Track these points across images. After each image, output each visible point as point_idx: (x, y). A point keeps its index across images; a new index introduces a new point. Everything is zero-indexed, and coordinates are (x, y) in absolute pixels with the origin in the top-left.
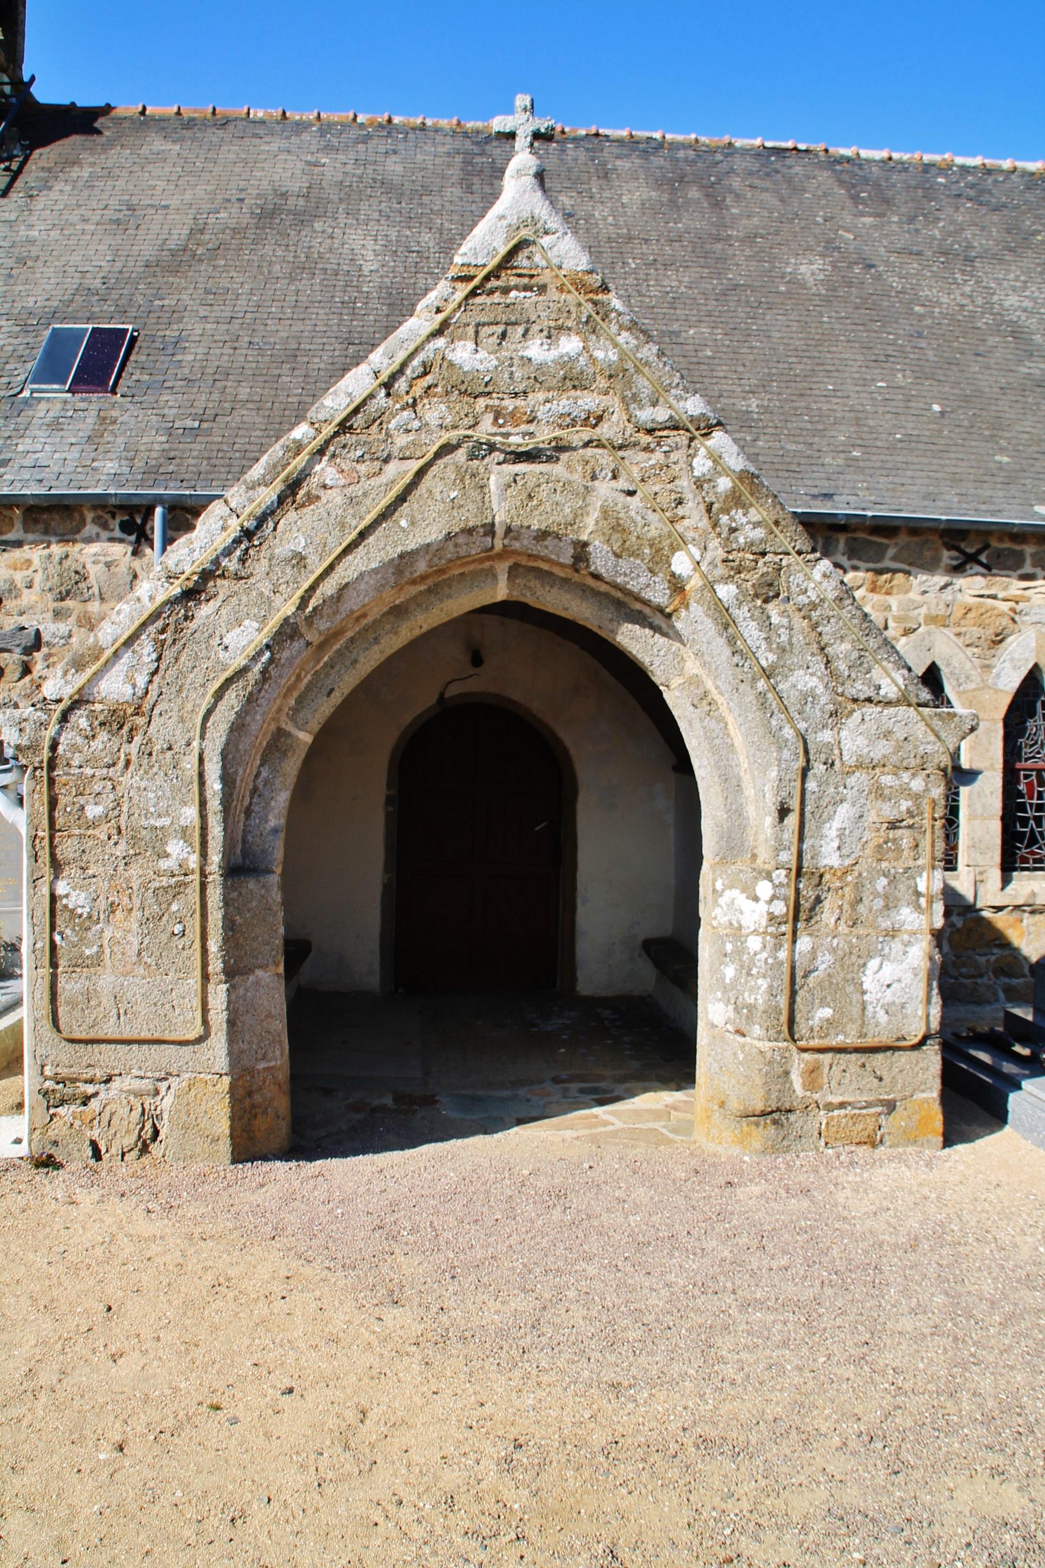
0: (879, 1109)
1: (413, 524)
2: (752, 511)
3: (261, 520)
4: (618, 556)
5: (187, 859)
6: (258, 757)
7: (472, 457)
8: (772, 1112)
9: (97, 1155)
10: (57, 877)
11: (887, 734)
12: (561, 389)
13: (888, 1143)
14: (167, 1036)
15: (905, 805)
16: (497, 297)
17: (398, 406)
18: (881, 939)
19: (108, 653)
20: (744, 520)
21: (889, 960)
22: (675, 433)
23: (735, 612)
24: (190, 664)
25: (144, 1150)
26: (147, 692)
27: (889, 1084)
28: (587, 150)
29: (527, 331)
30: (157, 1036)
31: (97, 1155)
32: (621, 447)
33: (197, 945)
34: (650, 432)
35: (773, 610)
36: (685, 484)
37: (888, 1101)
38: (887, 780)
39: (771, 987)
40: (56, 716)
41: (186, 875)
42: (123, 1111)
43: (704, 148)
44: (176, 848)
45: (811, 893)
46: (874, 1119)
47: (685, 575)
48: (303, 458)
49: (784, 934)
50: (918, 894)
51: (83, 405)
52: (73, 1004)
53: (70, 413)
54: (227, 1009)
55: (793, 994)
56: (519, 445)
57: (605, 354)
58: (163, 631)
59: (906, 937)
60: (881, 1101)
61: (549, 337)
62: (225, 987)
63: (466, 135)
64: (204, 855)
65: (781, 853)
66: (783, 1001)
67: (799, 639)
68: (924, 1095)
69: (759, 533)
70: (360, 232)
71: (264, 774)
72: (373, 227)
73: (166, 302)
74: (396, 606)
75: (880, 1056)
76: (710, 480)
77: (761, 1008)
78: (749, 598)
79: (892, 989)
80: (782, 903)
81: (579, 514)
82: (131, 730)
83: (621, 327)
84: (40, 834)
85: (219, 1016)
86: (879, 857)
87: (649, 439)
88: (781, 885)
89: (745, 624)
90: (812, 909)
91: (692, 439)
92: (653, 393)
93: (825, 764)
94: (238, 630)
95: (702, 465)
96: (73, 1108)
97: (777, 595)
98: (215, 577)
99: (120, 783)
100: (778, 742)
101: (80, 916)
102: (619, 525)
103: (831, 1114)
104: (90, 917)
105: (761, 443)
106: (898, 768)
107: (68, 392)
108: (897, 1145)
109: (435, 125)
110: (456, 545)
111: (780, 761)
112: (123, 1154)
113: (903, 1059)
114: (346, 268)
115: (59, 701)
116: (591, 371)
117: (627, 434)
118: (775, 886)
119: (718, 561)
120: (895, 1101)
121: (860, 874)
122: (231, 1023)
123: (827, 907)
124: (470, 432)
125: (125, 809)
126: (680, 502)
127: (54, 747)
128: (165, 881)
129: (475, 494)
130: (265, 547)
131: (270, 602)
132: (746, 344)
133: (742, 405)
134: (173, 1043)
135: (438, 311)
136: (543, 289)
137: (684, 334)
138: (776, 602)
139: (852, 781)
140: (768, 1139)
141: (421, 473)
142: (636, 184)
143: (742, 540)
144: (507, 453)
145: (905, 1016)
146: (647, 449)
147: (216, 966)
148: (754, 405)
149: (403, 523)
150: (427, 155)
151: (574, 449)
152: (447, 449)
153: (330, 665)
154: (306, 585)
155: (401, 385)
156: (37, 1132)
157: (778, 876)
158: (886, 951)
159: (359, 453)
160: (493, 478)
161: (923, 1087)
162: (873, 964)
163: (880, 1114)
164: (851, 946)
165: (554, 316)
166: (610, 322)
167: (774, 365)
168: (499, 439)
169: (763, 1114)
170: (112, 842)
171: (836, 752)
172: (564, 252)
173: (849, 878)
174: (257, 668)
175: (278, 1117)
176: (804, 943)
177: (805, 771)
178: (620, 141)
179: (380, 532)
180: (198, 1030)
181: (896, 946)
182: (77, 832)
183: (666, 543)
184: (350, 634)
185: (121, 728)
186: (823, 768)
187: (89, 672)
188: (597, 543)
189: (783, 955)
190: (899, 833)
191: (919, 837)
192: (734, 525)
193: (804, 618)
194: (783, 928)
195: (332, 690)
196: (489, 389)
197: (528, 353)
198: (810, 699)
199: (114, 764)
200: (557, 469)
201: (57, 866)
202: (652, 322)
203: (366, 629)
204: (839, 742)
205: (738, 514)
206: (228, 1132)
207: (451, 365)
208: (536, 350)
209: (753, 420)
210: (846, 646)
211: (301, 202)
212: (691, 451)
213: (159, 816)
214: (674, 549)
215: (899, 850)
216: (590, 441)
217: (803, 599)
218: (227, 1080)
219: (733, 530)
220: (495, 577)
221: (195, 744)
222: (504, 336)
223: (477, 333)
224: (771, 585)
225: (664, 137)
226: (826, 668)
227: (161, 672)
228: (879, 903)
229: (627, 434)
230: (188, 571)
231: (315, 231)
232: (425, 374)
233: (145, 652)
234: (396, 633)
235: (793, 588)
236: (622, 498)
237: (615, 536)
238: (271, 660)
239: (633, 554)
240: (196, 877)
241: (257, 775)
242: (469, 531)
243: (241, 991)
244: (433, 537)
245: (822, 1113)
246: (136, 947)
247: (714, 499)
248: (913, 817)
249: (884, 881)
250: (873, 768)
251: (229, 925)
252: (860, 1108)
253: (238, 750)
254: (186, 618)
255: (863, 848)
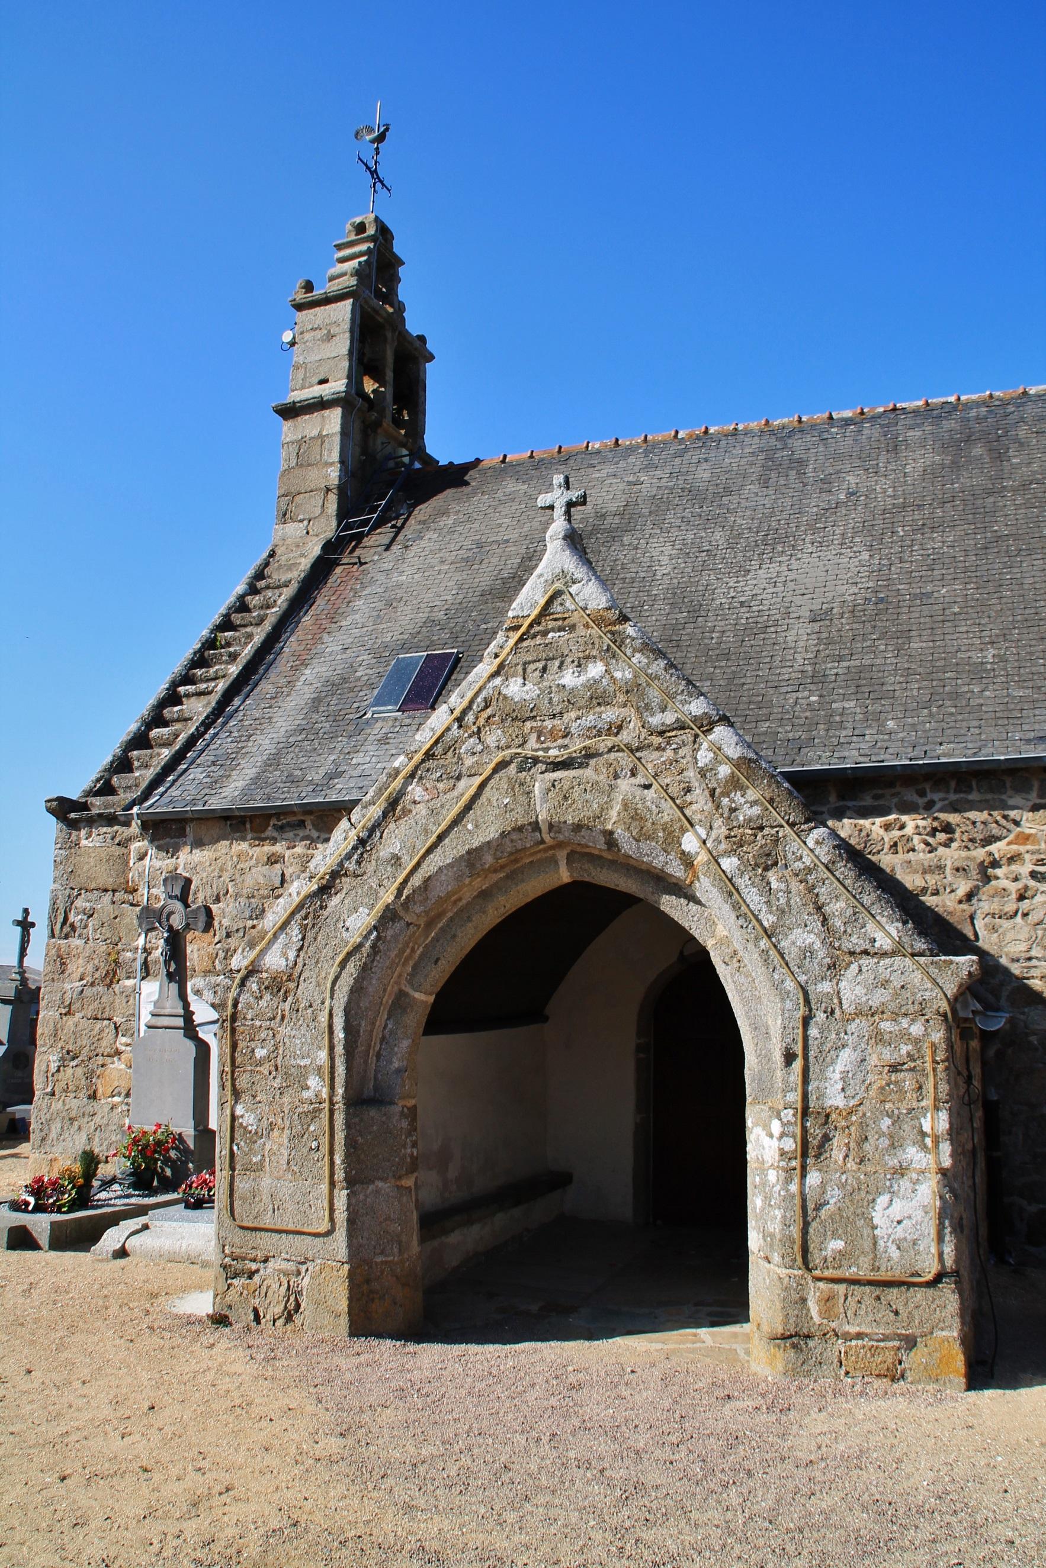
0: (897, 1343)
1: (477, 826)
2: (750, 792)
3: (371, 831)
4: (638, 841)
5: (321, 1091)
6: (386, 1013)
7: (521, 769)
8: (791, 1336)
9: (257, 1319)
10: (236, 1102)
11: (885, 984)
12: (588, 708)
13: (910, 1379)
14: (305, 1230)
15: (904, 1049)
16: (539, 640)
17: (466, 735)
18: (888, 1177)
19: (270, 935)
20: (742, 800)
21: (898, 1197)
22: (682, 732)
23: (738, 881)
24: (323, 942)
25: (289, 1319)
26: (296, 964)
27: (905, 1319)
28: (882, 426)
29: (562, 663)
30: (299, 1228)
31: (257, 1319)
32: (638, 749)
33: (326, 1158)
34: (661, 733)
35: (772, 876)
36: (692, 774)
37: (907, 1336)
38: (886, 1026)
39: (784, 1217)
40: (237, 981)
41: (320, 1103)
42: (275, 1286)
43: (997, 403)
44: (313, 1082)
45: (818, 1131)
46: (892, 1353)
47: (693, 852)
48: (400, 780)
49: (795, 1169)
50: (923, 1134)
51: (408, 721)
52: (244, 1199)
53: (397, 729)
54: (347, 1209)
55: (806, 1225)
56: (556, 757)
57: (623, 674)
58: (306, 918)
59: (914, 1176)
60: (899, 1335)
61: (579, 666)
62: (345, 1192)
63: (772, 433)
64: (332, 1087)
65: (788, 1094)
66: (795, 1231)
67: (796, 900)
68: (944, 1333)
69: (756, 810)
70: (661, 539)
71: (390, 1026)
72: (675, 533)
73: (489, 625)
74: (483, 891)
75: (895, 1291)
76: (712, 769)
77: (778, 1236)
78: (750, 868)
79: (902, 1225)
80: (792, 1140)
81: (604, 809)
82: (286, 992)
83: (634, 651)
84: (226, 1069)
85: (341, 1216)
86: (882, 1098)
87: (660, 740)
88: (789, 1123)
89: (747, 890)
90: (821, 1146)
91: (696, 736)
92: (662, 701)
93: (825, 1012)
94: (355, 915)
95: (704, 757)
96: (243, 1280)
97: (776, 864)
98: (341, 876)
99: (278, 1032)
100: (781, 994)
101: (250, 1132)
102: (637, 814)
103: (848, 1343)
104: (256, 1133)
105: (987, 693)
106: (897, 1015)
107: (398, 711)
108: (919, 1381)
109: (745, 428)
110: (512, 841)
111: (783, 1010)
112: (274, 1321)
113: (919, 1295)
114: (642, 575)
115: (239, 971)
116: (612, 689)
117: (642, 738)
118: (783, 1125)
119: (722, 837)
120: (916, 1337)
121: (864, 1115)
122: (351, 1221)
123: (835, 1144)
124: (519, 750)
125: (281, 1052)
126: (688, 790)
127: (235, 1005)
128: (306, 1107)
129: (522, 799)
130: (374, 851)
131: (377, 893)
132: (996, 595)
133: (976, 657)
134: (309, 1234)
135: (496, 656)
136: (573, 628)
137: (936, 595)
138: (775, 869)
139: (852, 1027)
140: (788, 1362)
141: (482, 786)
142: (923, 452)
143: (741, 818)
144: (548, 764)
145: (918, 1253)
146: (659, 748)
147: (340, 1175)
148: (990, 656)
149: (470, 827)
150: (734, 458)
151: (601, 755)
152: (502, 765)
153: (436, 939)
154: (400, 879)
155: (470, 717)
156: (219, 1297)
157: (786, 1115)
158: (896, 1188)
159: (438, 774)
160: (537, 784)
161: (941, 1325)
162: (883, 1200)
163: (899, 1349)
164: (859, 1182)
165: (581, 648)
166: (626, 646)
167: (1020, 612)
168: (540, 753)
169: (784, 1338)
170: (272, 1076)
171: (836, 1001)
172: (590, 595)
173: (854, 1118)
174: (368, 944)
175: (395, 1303)
176: (814, 1178)
177: (806, 1021)
178: (915, 412)
179: (453, 835)
180: (324, 1226)
181: (905, 1184)
182: (249, 1068)
183: (676, 826)
184: (450, 914)
185: (279, 991)
186: (823, 1016)
187: (258, 948)
188: (619, 831)
189: (794, 1188)
190: (901, 1075)
191: (921, 1080)
192: (733, 805)
193: (801, 882)
194: (794, 1163)
195: (438, 959)
196: (534, 713)
197: (562, 682)
198: (808, 954)
199: (274, 1018)
200: (588, 773)
201: (236, 1094)
202: (907, 587)
203: (461, 910)
204: (838, 992)
205: (738, 797)
206: (346, 1309)
207: (505, 697)
208: (569, 678)
209: (986, 670)
210: (841, 905)
211: (617, 520)
212: (696, 746)
213: (303, 1058)
214: (683, 831)
215: (901, 1091)
216: (613, 747)
217: (799, 865)
218: (347, 1267)
219: (733, 810)
220: (556, 863)
221: (327, 1003)
222: (544, 669)
223: (524, 670)
224: (768, 855)
225: (959, 399)
226: (823, 926)
227: (305, 948)
228: (884, 1142)
229: (642, 738)
230: (322, 870)
231: (623, 545)
232: (487, 707)
233: (294, 933)
234: (484, 912)
235: (789, 855)
236: (639, 792)
237: (634, 824)
238: (378, 938)
239: (649, 838)
240: (326, 1105)
241: (386, 1026)
242: (520, 829)
243: (361, 1197)
244: (492, 836)
245: (840, 1341)
246: (286, 1157)
247: (716, 785)
248: (914, 1060)
249: (887, 1121)
250: (872, 1016)
251: (351, 1144)
252: (878, 1341)
253: (359, 1007)
254: (321, 907)
255: (867, 1090)
